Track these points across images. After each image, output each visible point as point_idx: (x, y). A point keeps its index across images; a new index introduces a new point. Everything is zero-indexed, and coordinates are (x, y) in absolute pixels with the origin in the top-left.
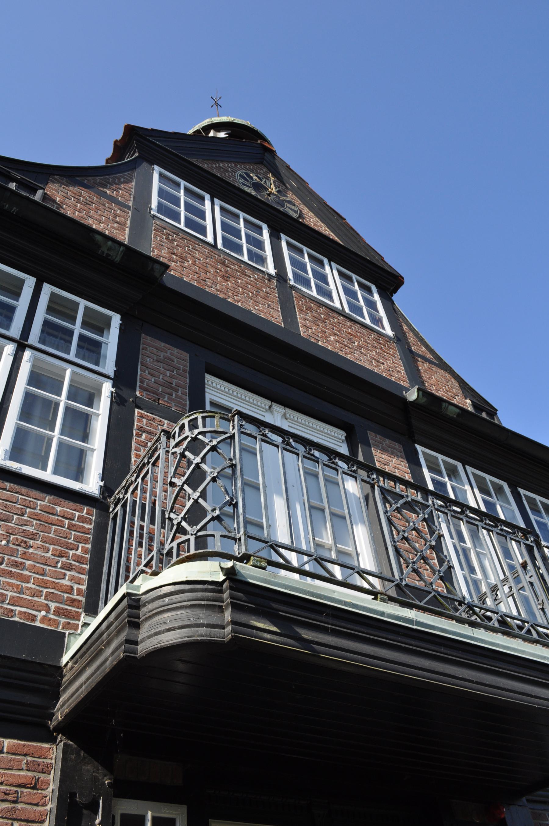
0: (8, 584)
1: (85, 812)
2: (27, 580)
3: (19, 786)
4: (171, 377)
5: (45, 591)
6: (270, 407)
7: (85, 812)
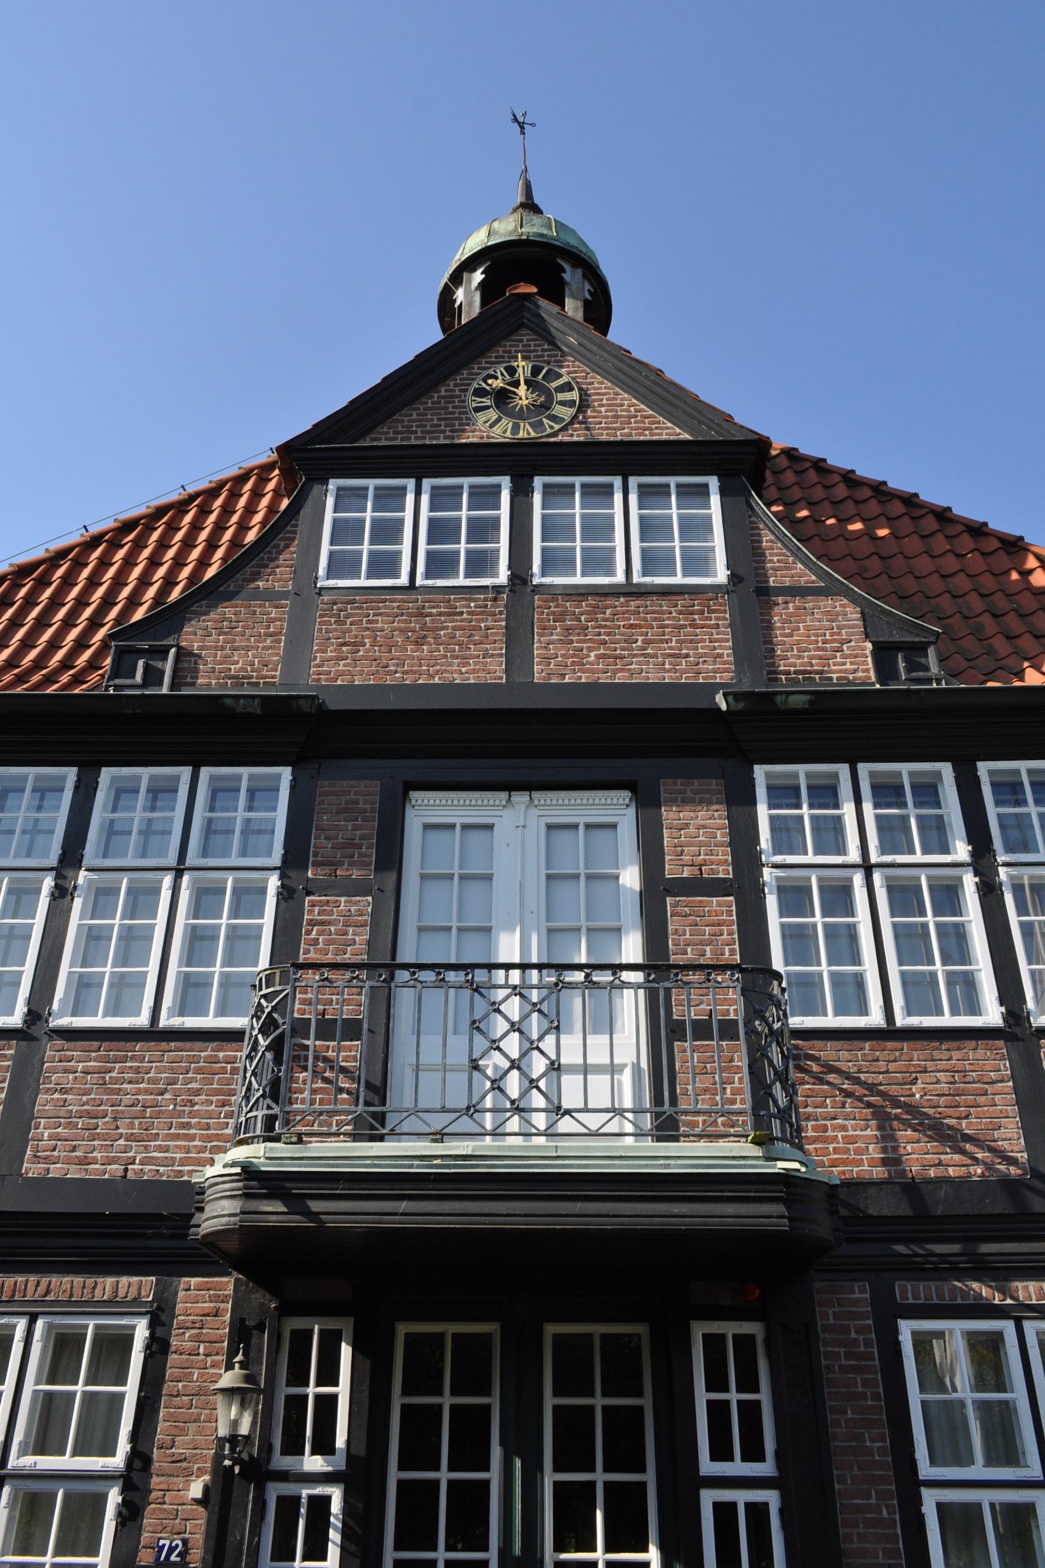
0: (176, 1146)
1: (254, 1332)
2: (192, 1138)
3: (203, 1315)
4: (355, 828)
5: (209, 1145)
6: (509, 800)
7: (254, 1332)
